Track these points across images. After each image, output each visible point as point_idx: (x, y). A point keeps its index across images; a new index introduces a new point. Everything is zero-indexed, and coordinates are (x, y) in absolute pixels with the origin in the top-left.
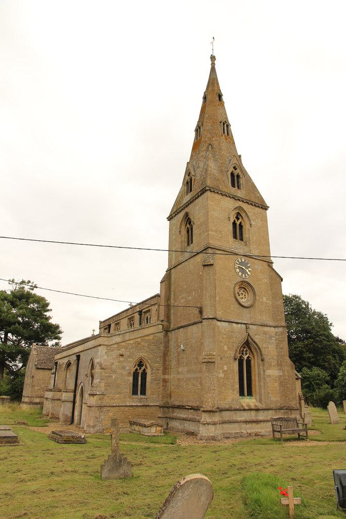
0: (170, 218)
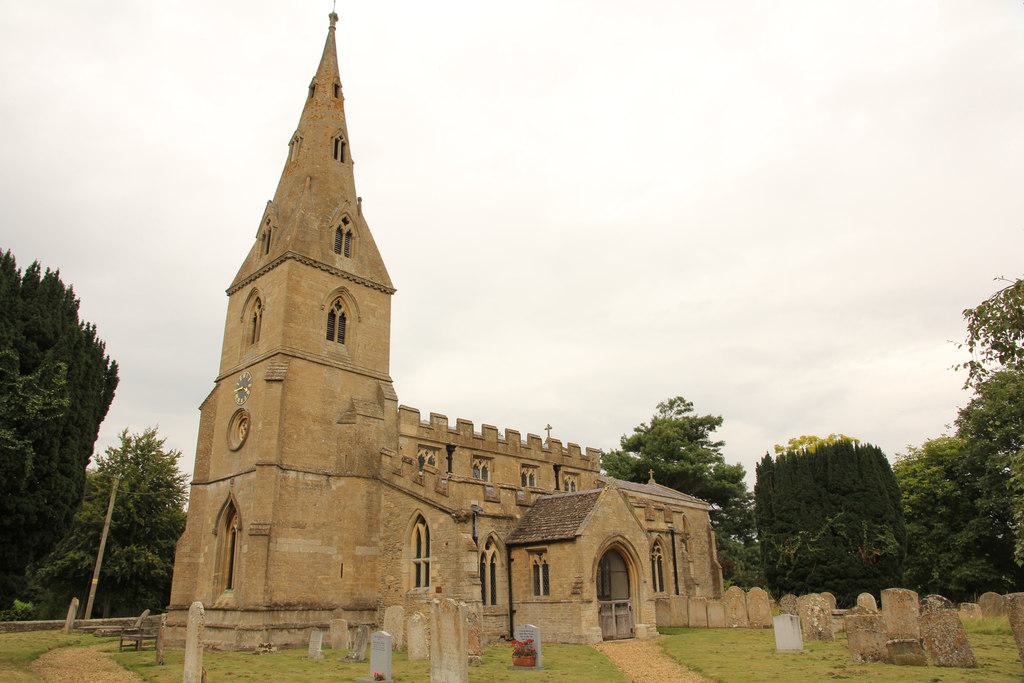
0: (231, 292)
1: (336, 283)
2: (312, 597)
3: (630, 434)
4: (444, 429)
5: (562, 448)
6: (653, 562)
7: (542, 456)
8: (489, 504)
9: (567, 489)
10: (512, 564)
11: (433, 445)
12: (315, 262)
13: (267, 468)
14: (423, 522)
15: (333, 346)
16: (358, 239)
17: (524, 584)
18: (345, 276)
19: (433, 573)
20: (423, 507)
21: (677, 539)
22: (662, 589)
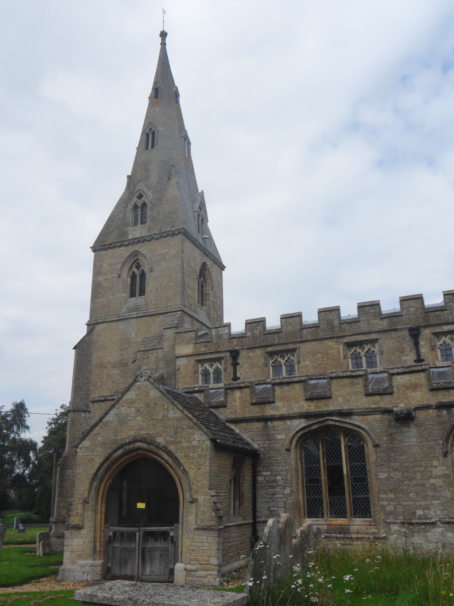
11: (213, 356)
12: (111, 244)
18: (136, 241)
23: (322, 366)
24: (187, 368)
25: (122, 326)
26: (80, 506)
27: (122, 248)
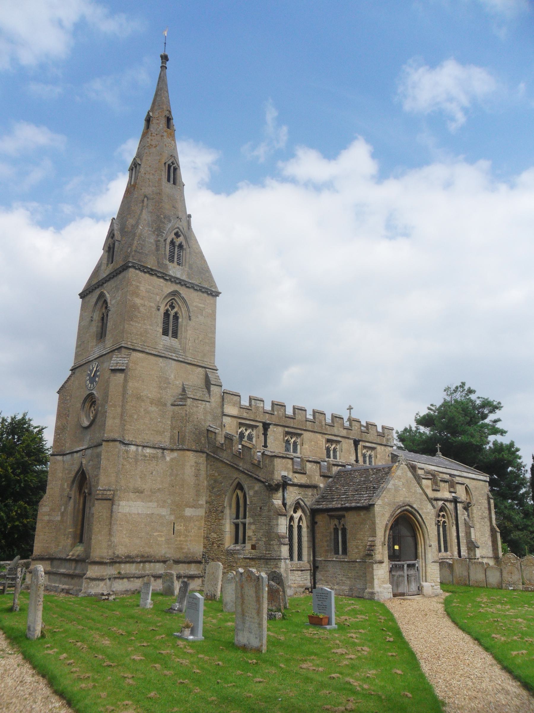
0: (83, 295)
1: (171, 287)
2: (148, 550)
3: (424, 412)
4: (261, 410)
5: (361, 426)
6: (438, 527)
7: (344, 433)
8: (297, 475)
9: (365, 462)
10: (316, 526)
12: (152, 270)
13: (111, 444)
14: (241, 488)
15: (168, 340)
16: (188, 250)
17: (325, 544)
18: (177, 281)
19: (249, 533)
20: (241, 476)
21: (460, 506)
22: (446, 550)
23: (314, 451)
24: (231, 427)
25: (161, 363)
26: (381, 547)
27: (161, 280)
